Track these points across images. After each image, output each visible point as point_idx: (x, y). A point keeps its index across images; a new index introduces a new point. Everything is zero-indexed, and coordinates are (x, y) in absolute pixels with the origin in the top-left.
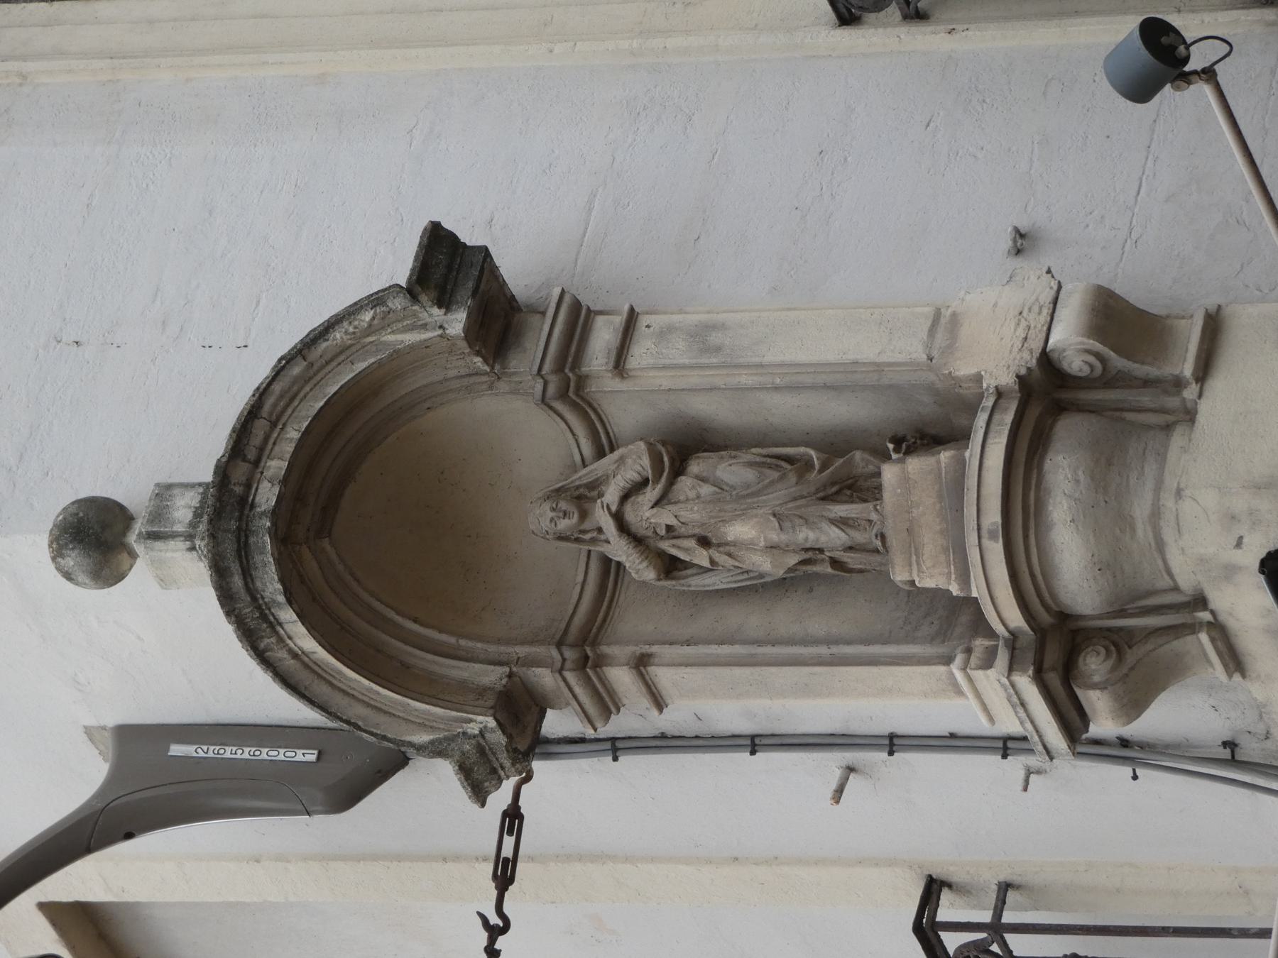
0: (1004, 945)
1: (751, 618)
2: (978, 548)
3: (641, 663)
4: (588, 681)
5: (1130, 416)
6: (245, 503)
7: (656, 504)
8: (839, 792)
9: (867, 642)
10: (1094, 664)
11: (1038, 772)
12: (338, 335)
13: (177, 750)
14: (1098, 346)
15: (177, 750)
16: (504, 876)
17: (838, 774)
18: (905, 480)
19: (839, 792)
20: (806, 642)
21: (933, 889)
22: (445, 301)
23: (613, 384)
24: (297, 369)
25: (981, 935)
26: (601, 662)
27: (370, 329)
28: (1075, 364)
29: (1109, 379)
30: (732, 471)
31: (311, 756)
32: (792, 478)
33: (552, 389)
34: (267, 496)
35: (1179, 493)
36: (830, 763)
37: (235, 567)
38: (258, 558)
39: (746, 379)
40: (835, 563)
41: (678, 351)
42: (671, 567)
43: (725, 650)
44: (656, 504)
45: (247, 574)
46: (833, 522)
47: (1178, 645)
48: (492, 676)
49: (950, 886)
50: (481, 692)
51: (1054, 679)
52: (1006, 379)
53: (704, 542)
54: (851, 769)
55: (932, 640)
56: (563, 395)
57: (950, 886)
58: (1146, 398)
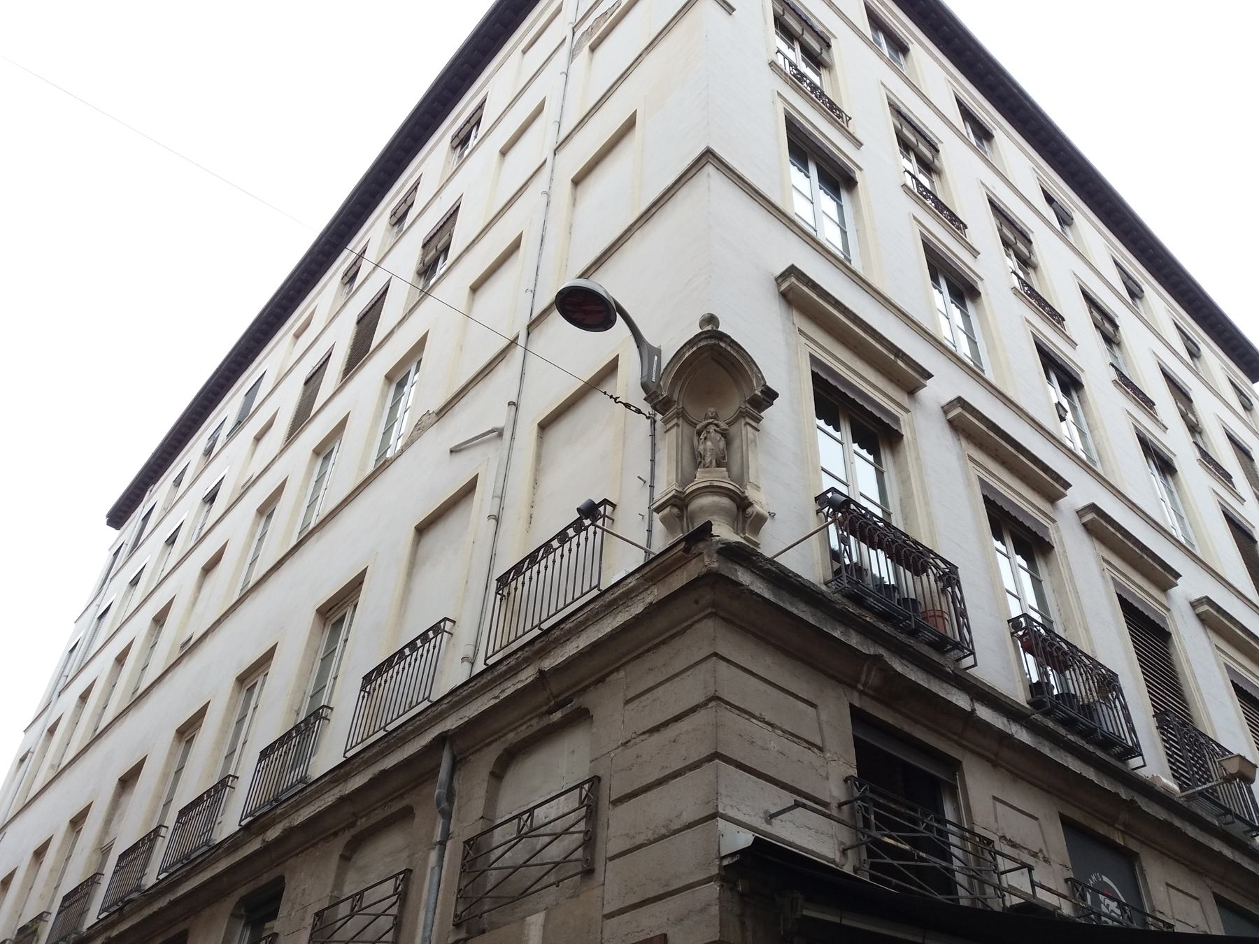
0: (600, 518)
1: (687, 448)
2: (530, 868)
3: (677, 425)
4: (674, 414)
5: (736, 523)
6: (721, 340)
7: (715, 430)
8: (640, 478)
9: (682, 470)
10: (675, 510)
11: (643, 518)
12: (756, 369)
13: (656, 358)
14: (754, 514)
15: (656, 358)
16: (627, 405)
17: (644, 479)
18: (722, 472)
19: (640, 478)
20: (682, 457)
21: (614, 506)
22: (762, 392)
23: (743, 423)
24: (749, 359)
25: (602, 513)
26: (678, 418)
27: (757, 376)
28: (750, 510)
29: (745, 518)
30: (722, 444)
31: (653, 380)
32: (721, 455)
33: (742, 410)
34: (722, 344)
35: (719, 525)
36: (647, 477)
37: (708, 335)
38: (709, 340)
39: (744, 448)
40: (701, 462)
41: (750, 436)
42: (699, 434)
43: (680, 441)
44: (715, 430)
45: (706, 338)
46: (711, 461)
47: (679, 531)
48: (675, 397)
49: (614, 510)
50: (672, 395)
51: (671, 502)
52: (747, 494)
53: (705, 438)
54: (645, 482)
55: (681, 480)
56: (741, 412)
57: (614, 510)
58: (740, 526)
